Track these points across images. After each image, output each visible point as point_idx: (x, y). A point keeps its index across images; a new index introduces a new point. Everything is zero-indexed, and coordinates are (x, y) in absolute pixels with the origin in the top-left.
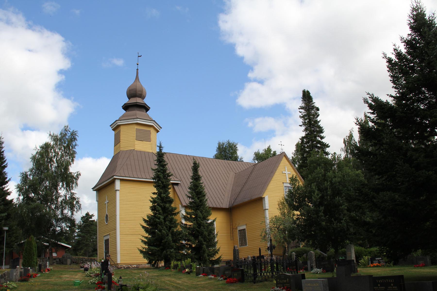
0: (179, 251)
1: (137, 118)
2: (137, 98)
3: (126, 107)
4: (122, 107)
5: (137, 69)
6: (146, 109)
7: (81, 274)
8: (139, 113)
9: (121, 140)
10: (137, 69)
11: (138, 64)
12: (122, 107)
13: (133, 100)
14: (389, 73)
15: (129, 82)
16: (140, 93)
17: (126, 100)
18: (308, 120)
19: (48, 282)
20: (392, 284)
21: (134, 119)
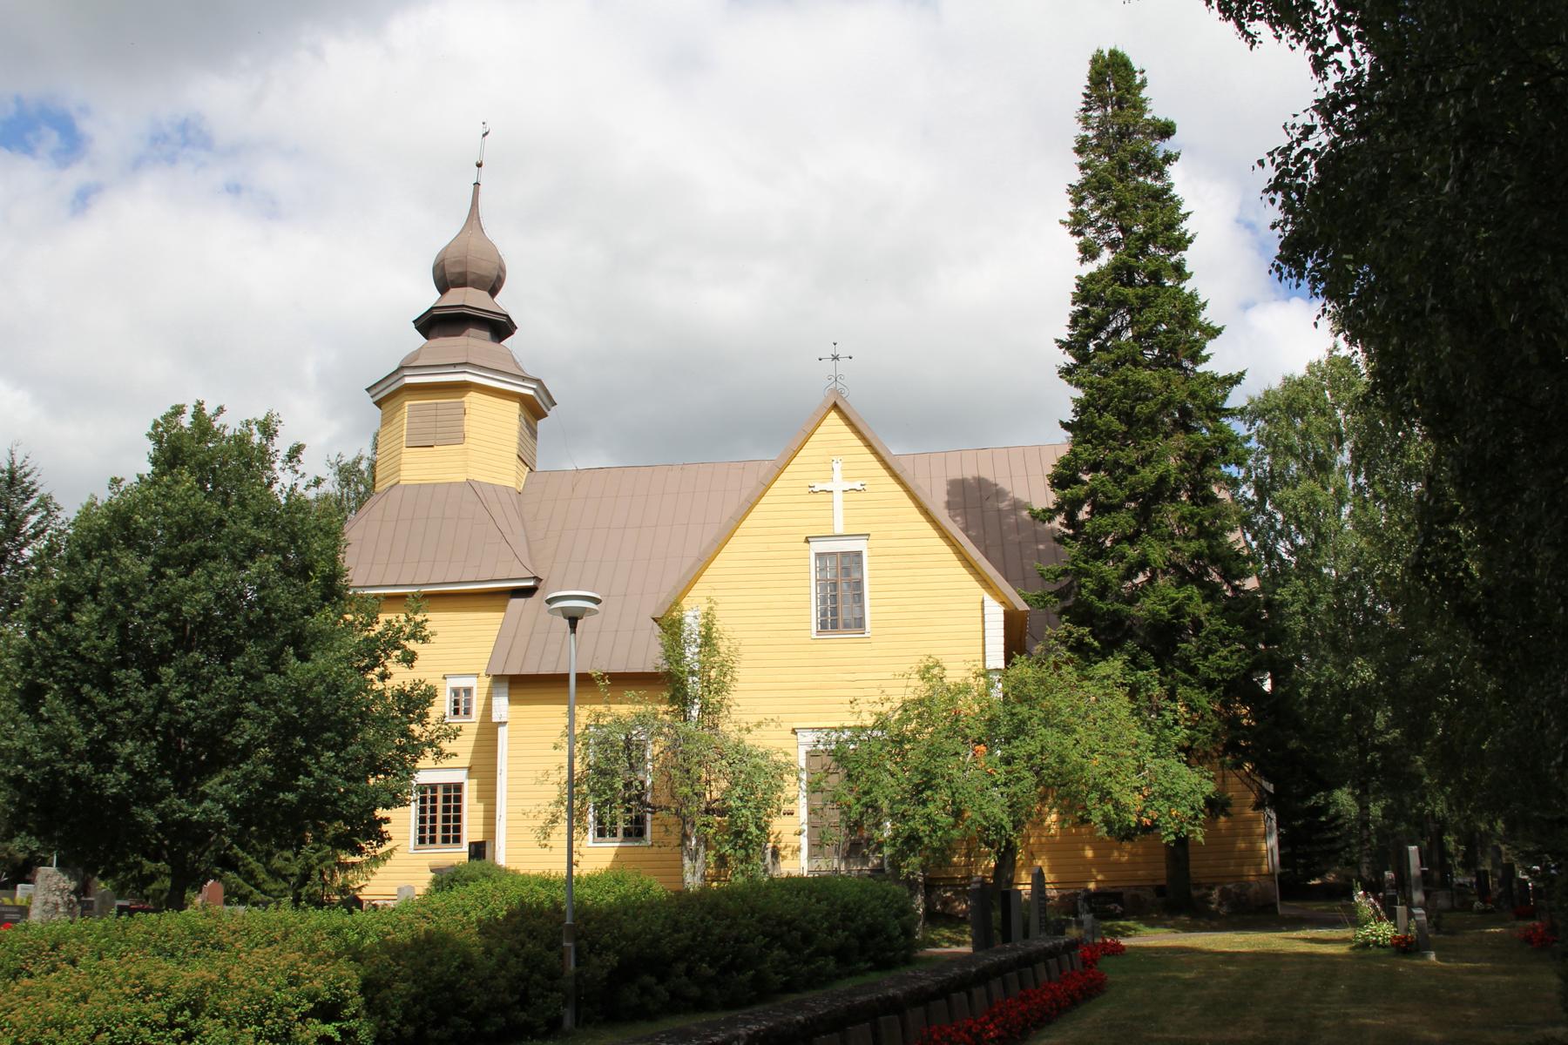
0: (1080, 420)
1: (465, 364)
2: (470, 290)
3: (431, 324)
4: (414, 322)
5: (477, 184)
6: (501, 328)
7: (618, 844)
8: (474, 343)
9: (402, 467)
10: (477, 184)
11: (479, 165)
12: (414, 322)
13: (456, 297)
14: (329, 470)
15: (440, 234)
16: (458, 269)
17: (428, 297)
18: (161, 739)
19: (943, 515)
20: (1087, 848)
21: (454, 365)
